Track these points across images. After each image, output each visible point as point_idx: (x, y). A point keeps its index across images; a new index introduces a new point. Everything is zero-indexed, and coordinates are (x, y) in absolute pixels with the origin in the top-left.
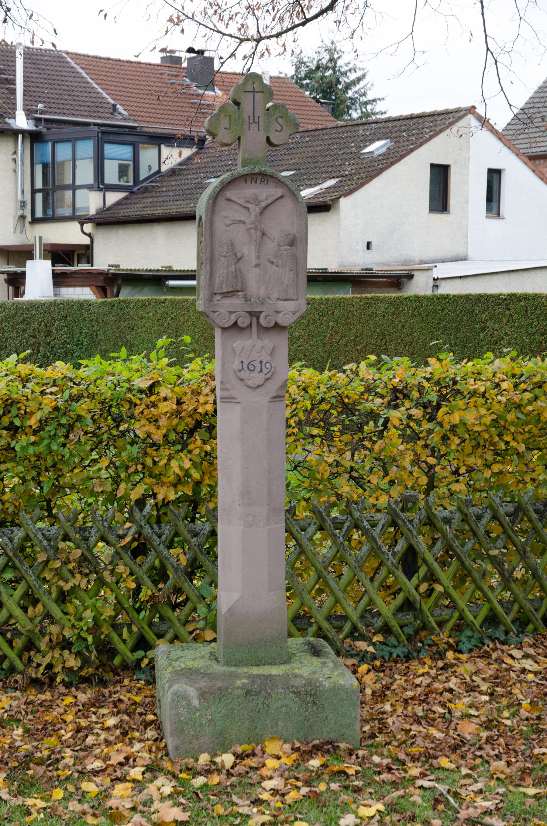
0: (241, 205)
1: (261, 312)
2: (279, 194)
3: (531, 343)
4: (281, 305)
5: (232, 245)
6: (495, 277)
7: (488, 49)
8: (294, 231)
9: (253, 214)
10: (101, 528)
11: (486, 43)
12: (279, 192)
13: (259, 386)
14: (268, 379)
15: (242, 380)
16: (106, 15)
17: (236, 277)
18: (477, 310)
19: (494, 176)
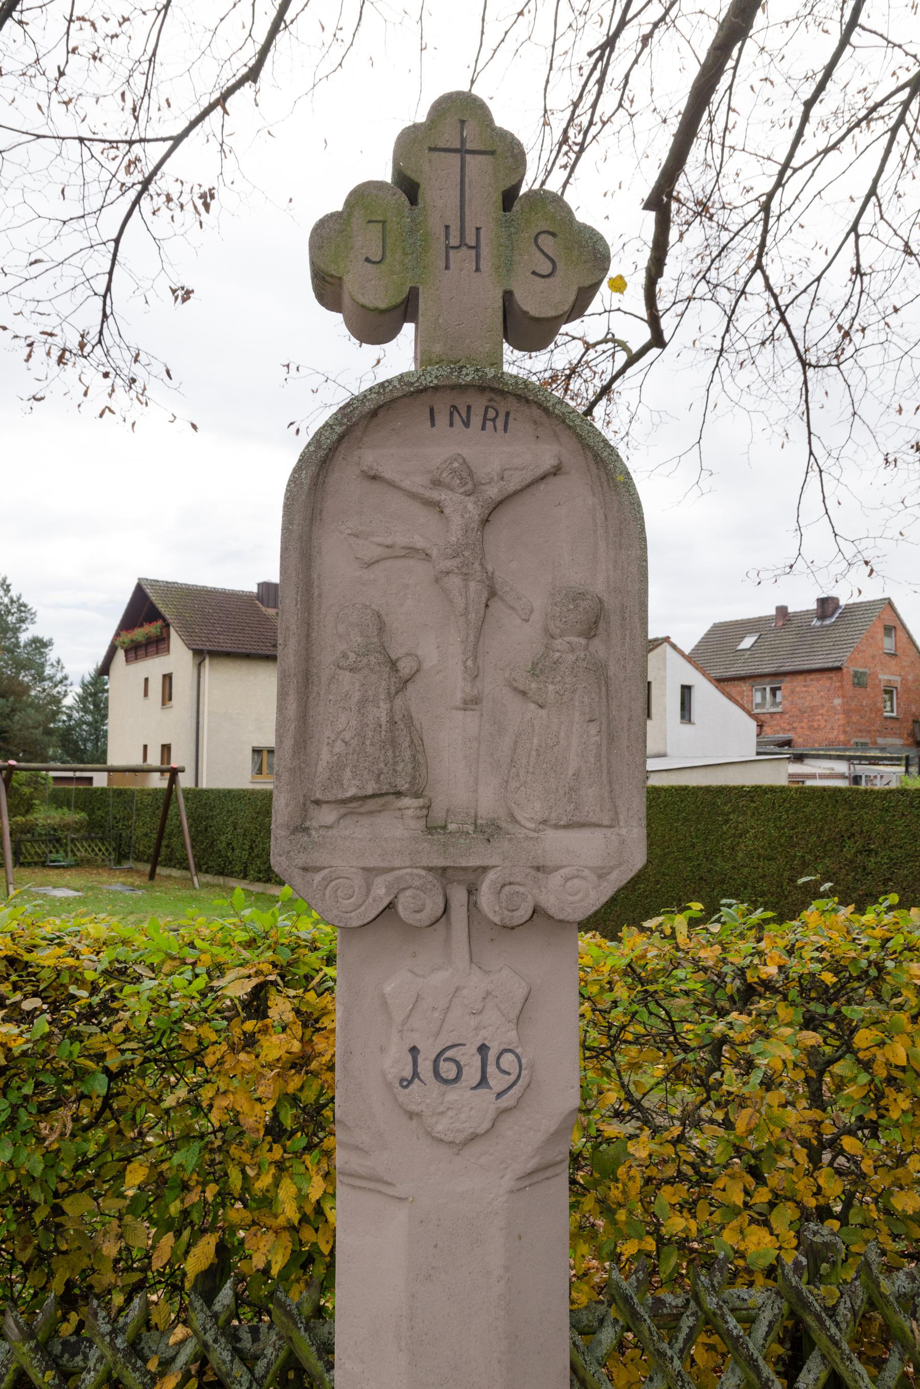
0: (413, 496)
1: (485, 869)
2: (548, 462)
3: (780, 837)
4: (557, 843)
5: (382, 628)
6: (733, 767)
7: (811, 453)
8: (599, 587)
9: (457, 521)
10: (108, 1353)
11: (810, 443)
12: (546, 455)
13: (474, 1137)
14: (506, 1110)
15: (411, 1115)
16: (298, 431)
17: (393, 742)
18: (719, 802)
19: (686, 690)
